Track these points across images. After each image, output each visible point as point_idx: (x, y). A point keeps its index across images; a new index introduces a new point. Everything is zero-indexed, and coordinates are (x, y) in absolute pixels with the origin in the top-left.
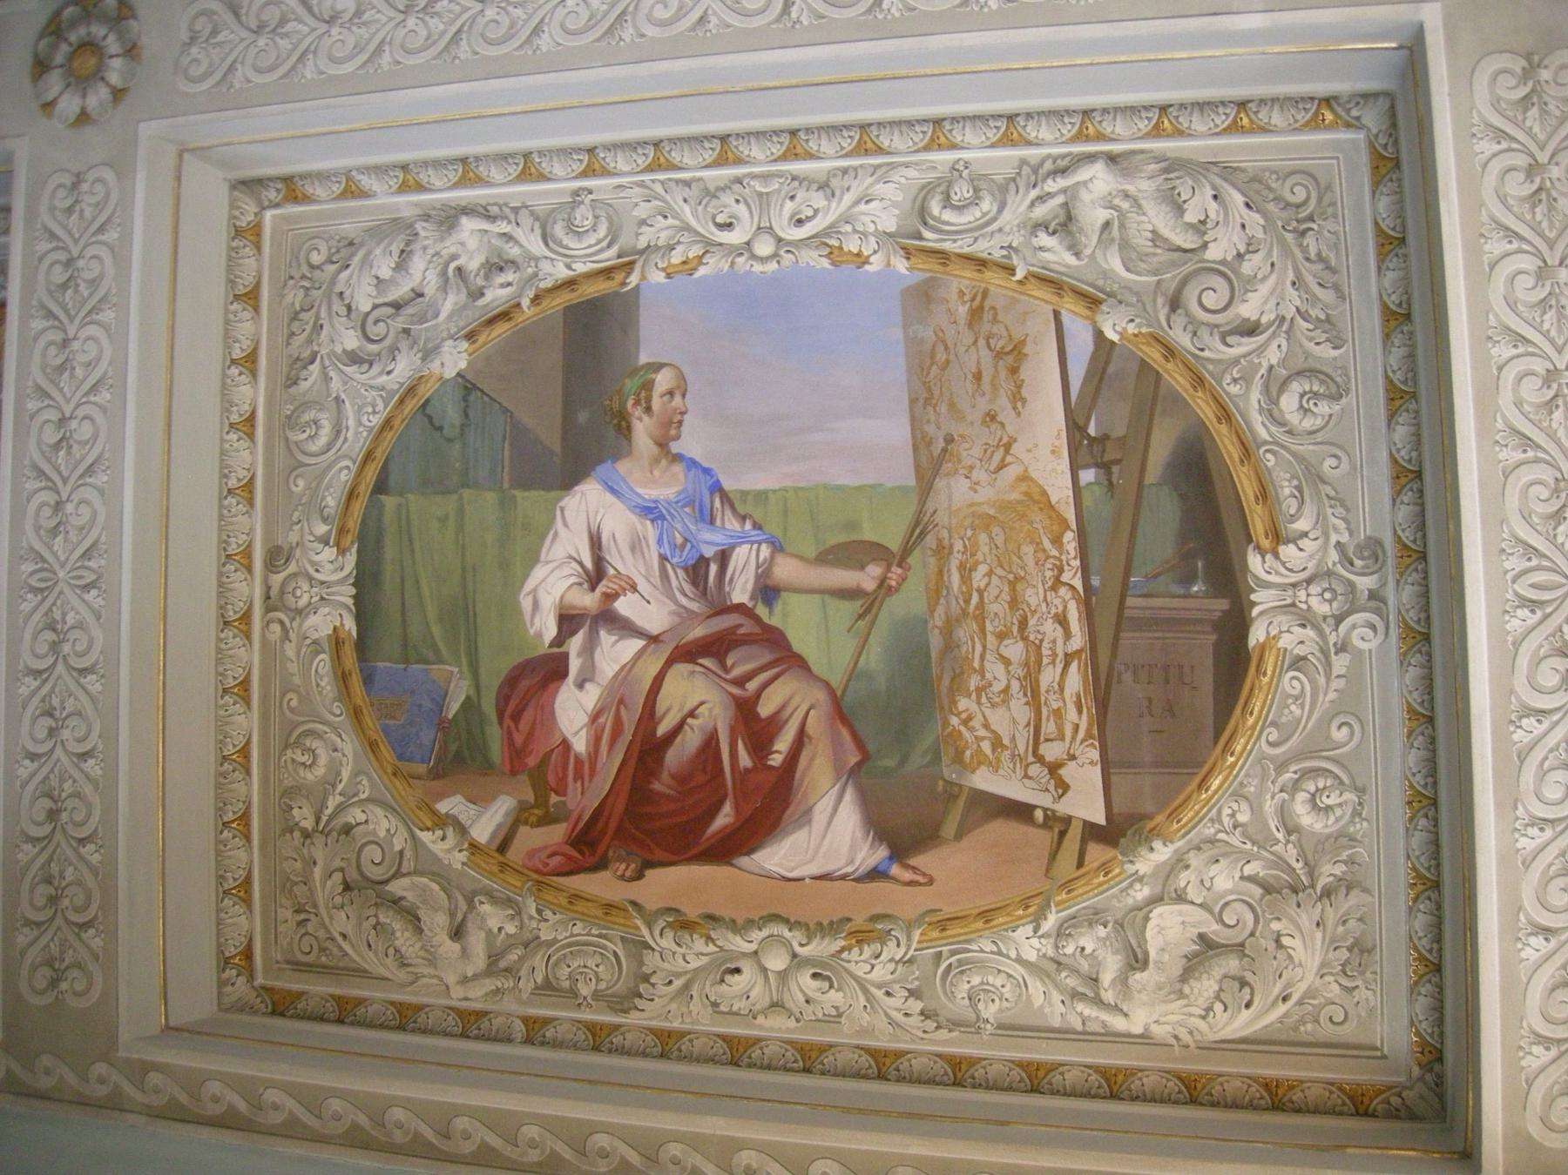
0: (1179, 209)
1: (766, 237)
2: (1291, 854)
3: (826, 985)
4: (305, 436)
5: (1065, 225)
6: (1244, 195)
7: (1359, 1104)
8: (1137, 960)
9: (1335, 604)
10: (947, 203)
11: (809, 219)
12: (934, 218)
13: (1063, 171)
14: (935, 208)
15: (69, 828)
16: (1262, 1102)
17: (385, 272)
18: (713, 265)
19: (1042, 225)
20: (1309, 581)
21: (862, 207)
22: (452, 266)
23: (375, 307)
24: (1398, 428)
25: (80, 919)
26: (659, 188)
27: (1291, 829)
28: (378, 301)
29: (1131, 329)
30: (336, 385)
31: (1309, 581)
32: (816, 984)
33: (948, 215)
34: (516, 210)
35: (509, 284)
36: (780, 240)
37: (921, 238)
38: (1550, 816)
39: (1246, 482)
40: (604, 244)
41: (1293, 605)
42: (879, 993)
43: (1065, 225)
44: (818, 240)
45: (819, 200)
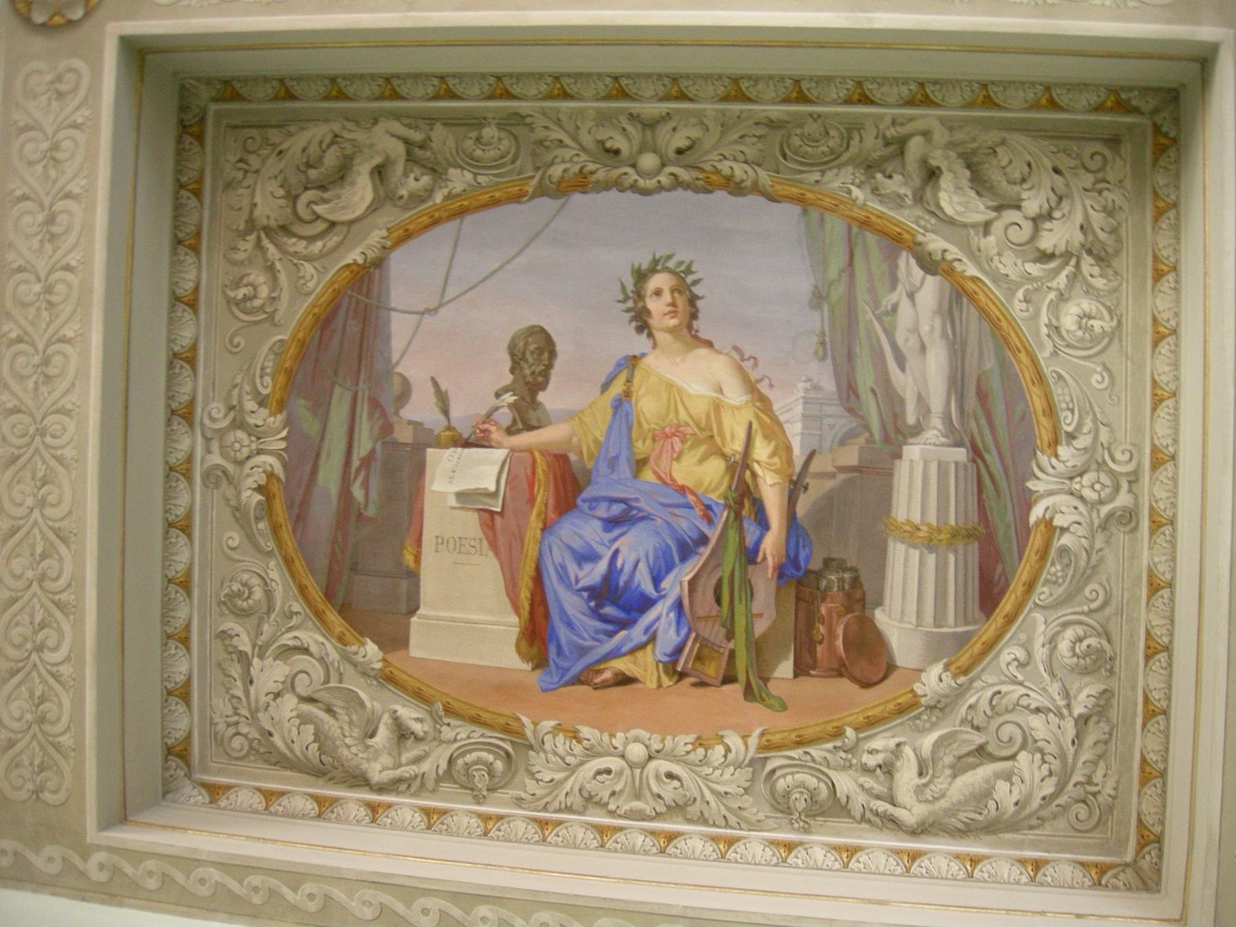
0: (317, 737)
1: (634, 759)
2: (272, 250)
3: (608, 145)
4: (1086, 643)
5: (402, 734)
6: (272, 744)
7: (658, 122)
8: (380, 173)
9: (233, 439)
10: (490, 767)
11: (599, 773)
12: (501, 758)
13: (400, 780)
14: (499, 765)
15: (32, 277)
16: (1059, 91)
17: (1002, 787)
18: (683, 742)
19: (418, 739)
20: (248, 458)
21: (559, 776)
22: (924, 780)
23: (1013, 757)
24: (183, 727)
25: (23, 347)
26: (733, 820)
27: (270, 269)
28: (1008, 764)
29: (354, 648)
30: (1054, 689)
31: (248, 458)
32: (616, 146)
33: (491, 758)
34: (863, 819)
35: (871, 752)
36: (623, 756)
37: (512, 742)
38: (57, 416)
39: (280, 512)
40: (779, 773)
41: (259, 439)
42: (567, 140)
43: (402, 734)
44: (592, 753)
45: (592, 787)
